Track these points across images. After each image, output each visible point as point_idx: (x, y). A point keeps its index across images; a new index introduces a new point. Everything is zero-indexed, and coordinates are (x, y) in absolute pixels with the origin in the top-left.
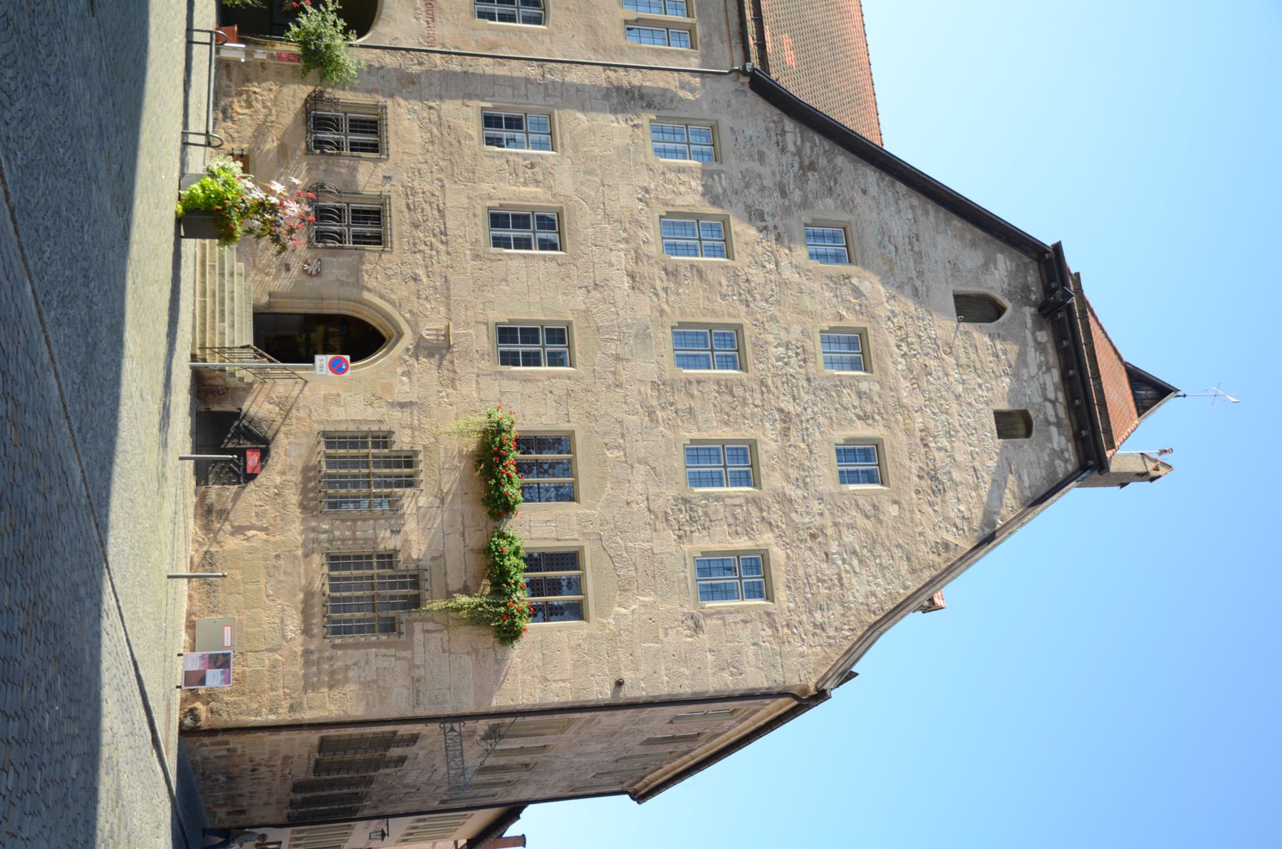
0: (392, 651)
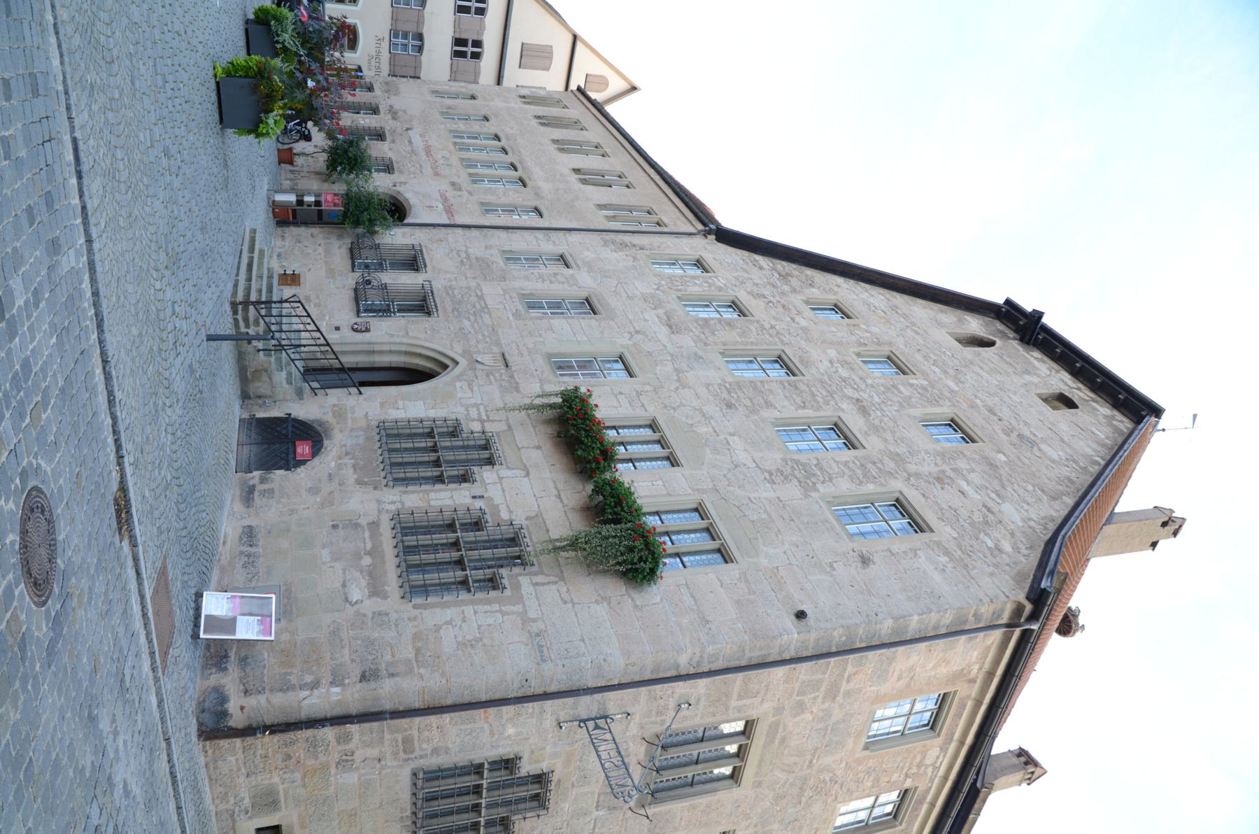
0: (496, 607)
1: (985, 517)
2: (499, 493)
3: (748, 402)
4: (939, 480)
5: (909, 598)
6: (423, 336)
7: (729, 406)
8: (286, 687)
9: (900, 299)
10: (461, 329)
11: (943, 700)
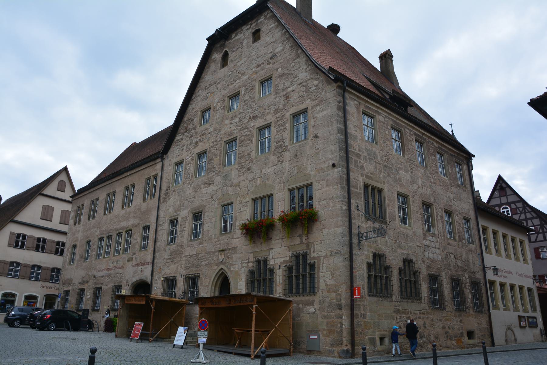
0: (321, 265)
1: (304, 86)
2: (279, 260)
3: (248, 162)
4: (287, 98)
5: (332, 126)
6: (208, 280)
7: (249, 169)
8: (341, 332)
9: (202, 84)
10: (206, 265)
11: (364, 113)
